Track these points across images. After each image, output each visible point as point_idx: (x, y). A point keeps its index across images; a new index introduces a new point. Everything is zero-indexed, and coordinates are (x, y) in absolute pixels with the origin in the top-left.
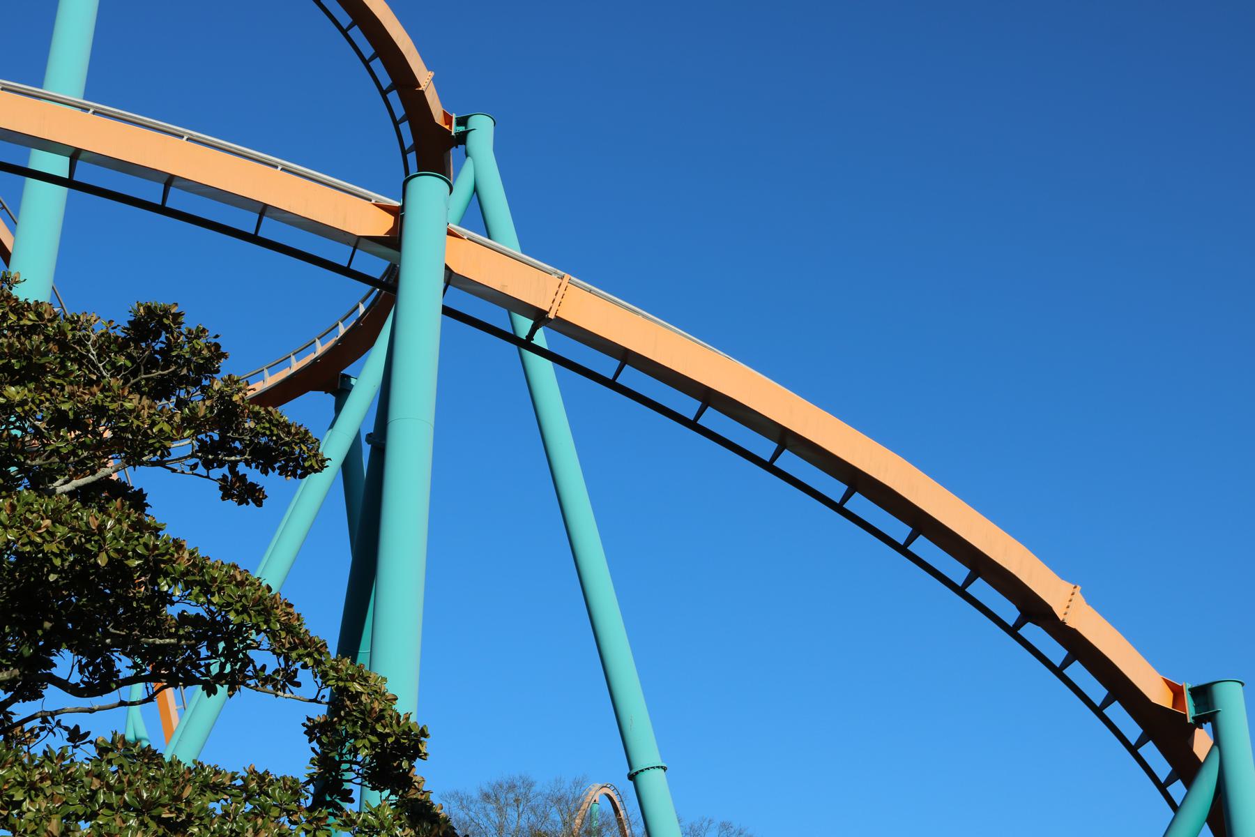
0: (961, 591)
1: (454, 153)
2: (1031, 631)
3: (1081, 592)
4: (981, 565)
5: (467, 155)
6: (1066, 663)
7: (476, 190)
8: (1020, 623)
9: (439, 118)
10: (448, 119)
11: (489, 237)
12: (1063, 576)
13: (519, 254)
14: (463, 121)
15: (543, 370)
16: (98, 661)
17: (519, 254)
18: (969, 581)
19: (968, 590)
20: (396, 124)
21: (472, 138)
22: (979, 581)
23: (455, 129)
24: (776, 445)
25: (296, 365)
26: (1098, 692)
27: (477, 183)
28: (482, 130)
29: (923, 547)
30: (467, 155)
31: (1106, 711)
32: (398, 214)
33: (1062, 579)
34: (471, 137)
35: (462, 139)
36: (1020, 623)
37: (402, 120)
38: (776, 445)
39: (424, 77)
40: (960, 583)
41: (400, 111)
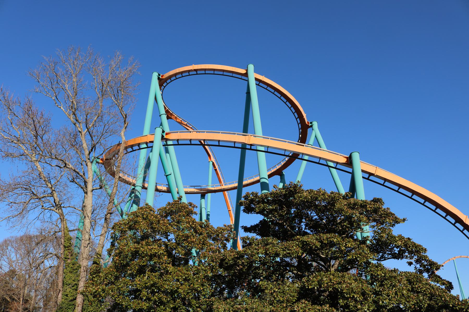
0: (434, 211)
1: (309, 130)
2: (457, 225)
3: (468, 217)
4: (414, 192)
5: (313, 130)
6: (446, 216)
7: (316, 136)
8: (455, 223)
9: (307, 123)
10: (308, 123)
11: (320, 148)
12: (465, 214)
13: (326, 150)
14: (311, 123)
15: (334, 171)
16: (266, 201)
17: (326, 150)
18: (424, 202)
19: (436, 211)
20: (294, 114)
21: (313, 126)
22: (427, 202)
23: (310, 125)
24: (384, 181)
25: (282, 163)
26: (434, 207)
27: (316, 135)
28: (315, 124)
29: (415, 197)
30: (313, 130)
31: (463, 232)
32: (247, 70)
33: (464, 214)
34: (313, 126)
35: (311, 126)
36: (455, 223)
37: (295, 112)
38: (384, 181)
39: (305, 115)
40: (434, 210)
41: (294, 111)
